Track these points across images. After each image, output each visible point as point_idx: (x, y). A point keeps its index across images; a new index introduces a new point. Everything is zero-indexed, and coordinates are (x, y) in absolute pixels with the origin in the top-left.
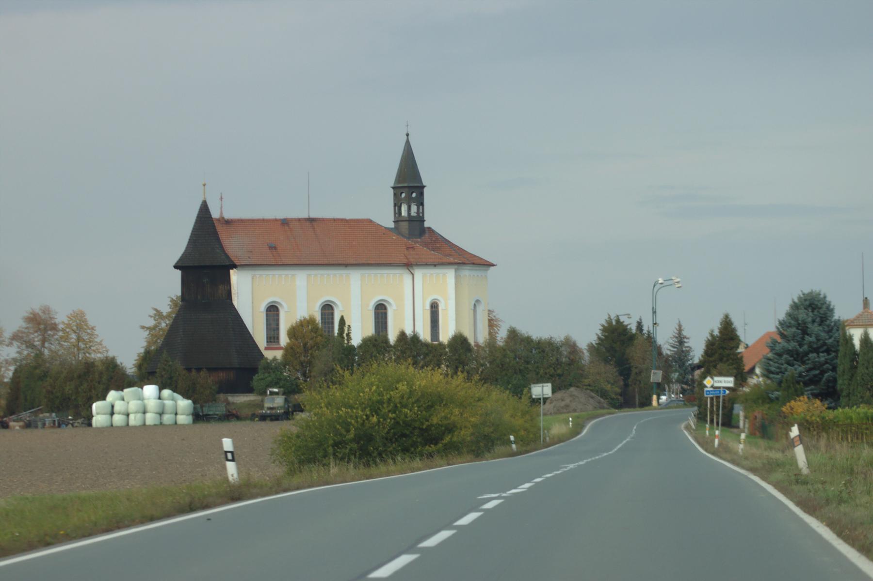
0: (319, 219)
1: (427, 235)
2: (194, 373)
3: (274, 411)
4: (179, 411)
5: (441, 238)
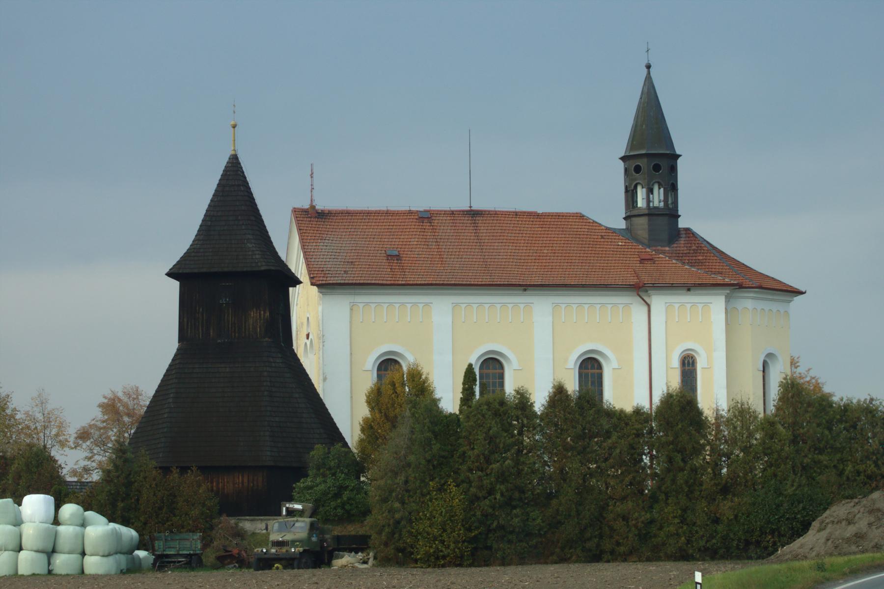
0: (489, 211)
1: (682, 241)
2: (175, 475)
3: (284, 550)
4: (88, 550)
5: (708, 246)
